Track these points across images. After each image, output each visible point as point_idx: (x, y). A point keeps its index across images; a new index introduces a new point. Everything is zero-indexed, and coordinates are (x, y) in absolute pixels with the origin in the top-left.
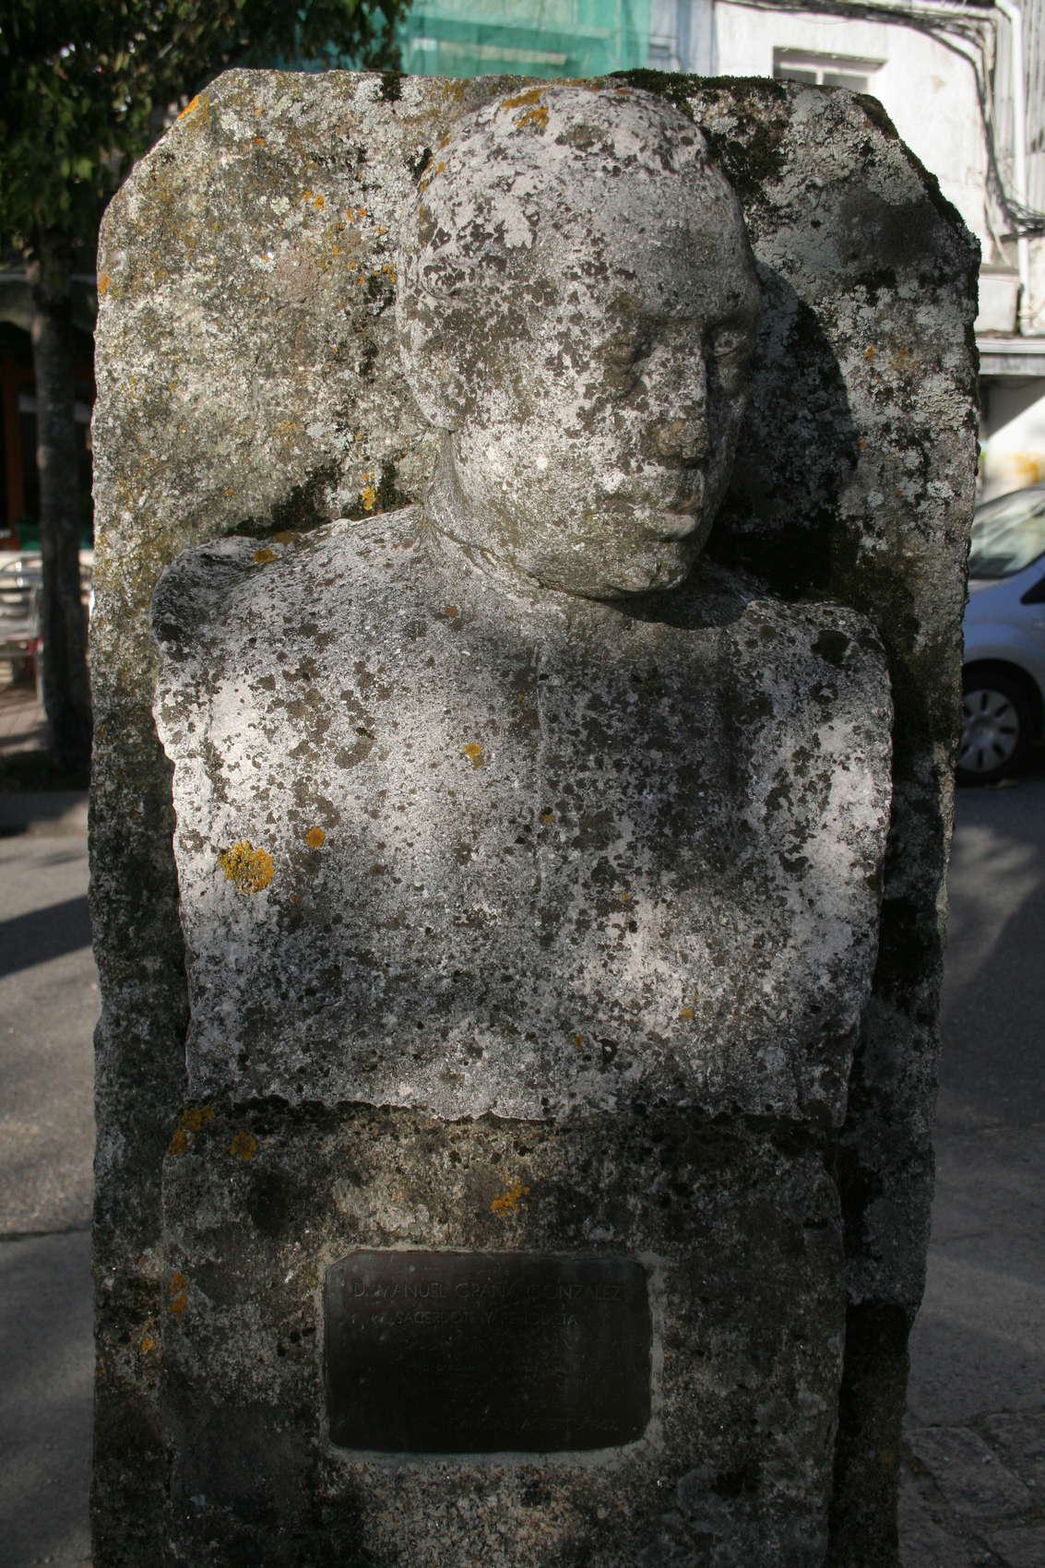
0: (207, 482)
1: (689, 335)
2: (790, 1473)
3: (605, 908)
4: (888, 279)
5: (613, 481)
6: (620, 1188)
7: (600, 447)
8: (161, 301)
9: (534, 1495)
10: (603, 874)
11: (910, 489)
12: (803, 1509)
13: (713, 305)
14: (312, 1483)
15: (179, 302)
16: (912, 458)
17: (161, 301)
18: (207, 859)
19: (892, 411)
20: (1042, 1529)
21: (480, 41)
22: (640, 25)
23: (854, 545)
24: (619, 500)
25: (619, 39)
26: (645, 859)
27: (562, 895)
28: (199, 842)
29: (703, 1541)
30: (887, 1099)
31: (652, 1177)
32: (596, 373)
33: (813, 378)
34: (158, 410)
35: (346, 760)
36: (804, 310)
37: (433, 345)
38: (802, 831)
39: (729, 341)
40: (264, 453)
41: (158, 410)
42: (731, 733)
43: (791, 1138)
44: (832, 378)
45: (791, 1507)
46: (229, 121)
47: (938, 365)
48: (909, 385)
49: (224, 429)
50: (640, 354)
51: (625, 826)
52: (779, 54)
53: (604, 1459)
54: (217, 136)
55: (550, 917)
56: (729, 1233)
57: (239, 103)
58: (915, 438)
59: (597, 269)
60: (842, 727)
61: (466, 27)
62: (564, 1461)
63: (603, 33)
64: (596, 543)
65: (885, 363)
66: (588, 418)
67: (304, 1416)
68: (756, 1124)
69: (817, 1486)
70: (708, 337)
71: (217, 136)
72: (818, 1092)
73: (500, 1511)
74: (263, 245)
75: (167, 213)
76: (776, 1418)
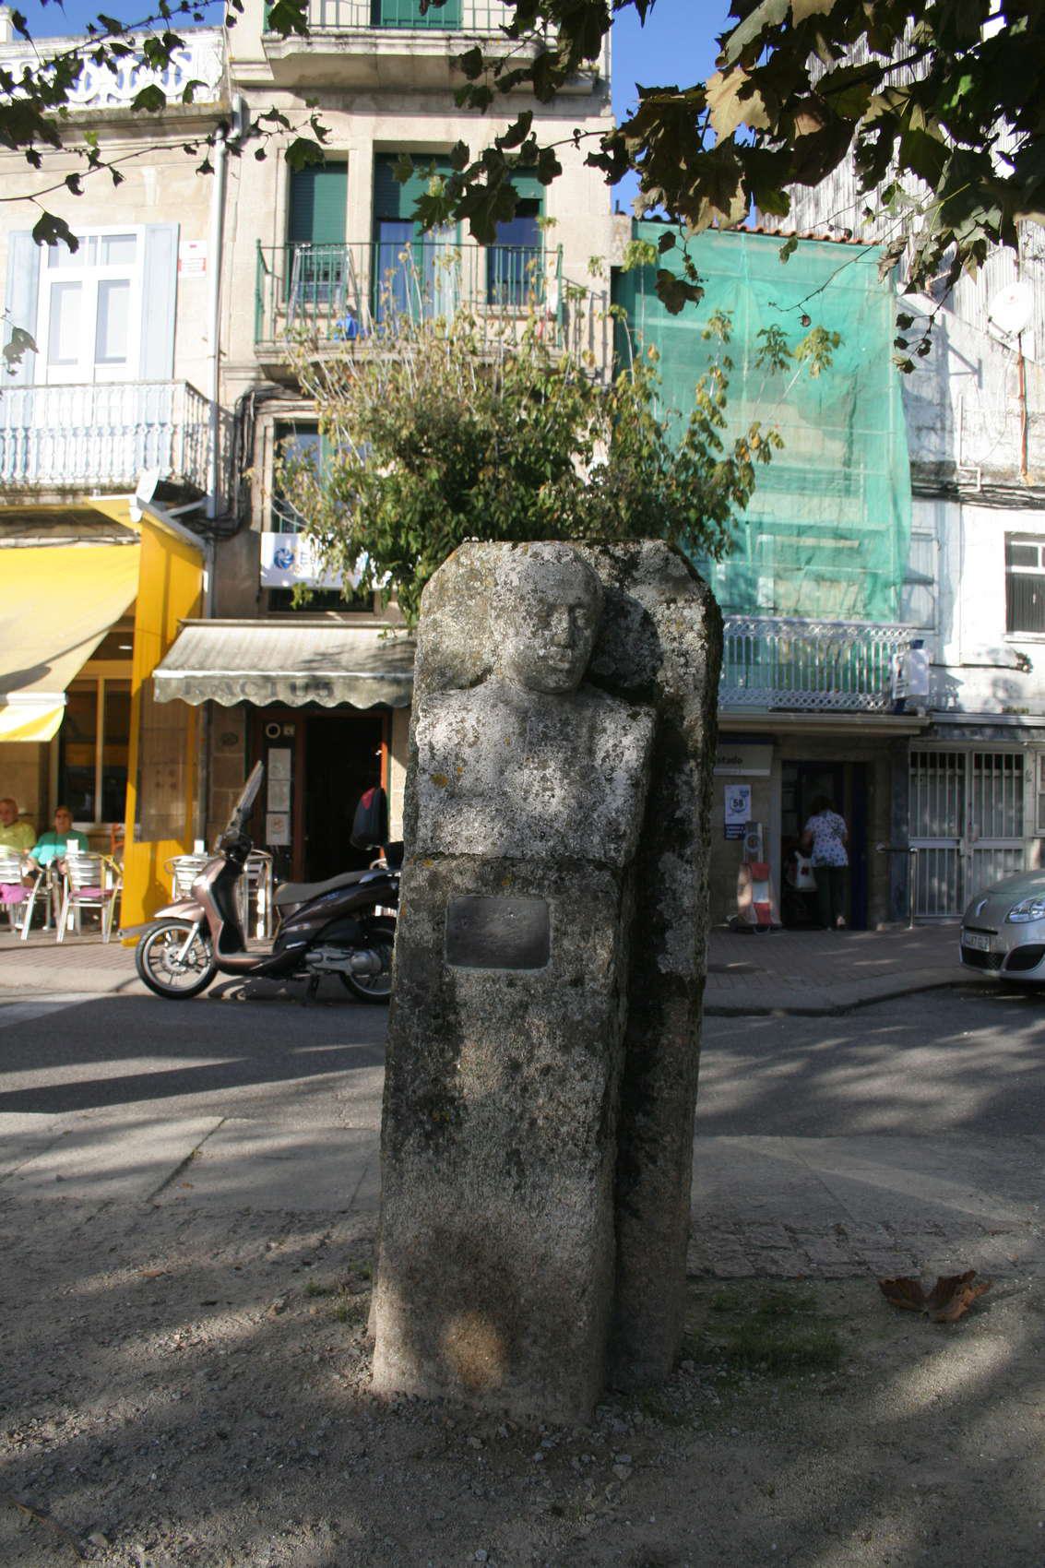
0: (449, 674)
1: (563, 609)
2: (594, 979)
3: (545, 790)
4: (674, 601)
5: (542, 652)
6: (542, 878)
7: (537, 642)
8: (438, 616)
9: (511, 984)
10: (544, 778)
11: (682, 671)
12: (599, 994)
13: (571, 600)
14: (441, 976)
15: (444, 616)
16: (682, 660)
17: (438, 616)
18: (426, 777)
19: (675, 644)
20: (1041, 1410)
21: (799, 535)
22: (906, 522)
23: (662, 690)
24: (544, 658)
25: (892, 530)
26: (558, 775)
27: (531, 785)
28: (424, 771)
29: (565, 1003)
30: (674, 892)
31: (553, 876)
32: (536, 620)
33: (648, 634)
34: (435, 651)
35: (470, 746)
36: (646, 613)
37: (498, 617)
38: (613, 769)
39: (579, 612)
40: (468, 664)
41: (435, 651)
42: (591, 738)
43: (600, 866)
44: (654, 634)
45: (595, 993)
46: (463, 559)
47: (692, 629)
48: (682, 636)
49: (456, 656)
50: (549, 615)
51: (552, 764)
52: (1009, 536)
53: (535, 972)
54: (458, 563)
55: (526, 792)
56: (575, 893)
57: (466, 553)
58: (684, 654)
59: (535, 591)
60: (630, 737)
61: (790, 527)
62: (521, 972)
63: (882, 527)
64: (539, 672)
65: (673, 629)
66: (534, 634)
67: (439, 953)
68: (589, 861)
69: (603, 985)
70: (571, 610)
71: (458, 563)
72: (613, 854)
73: (499, 990)
74: (471, 597)
75: (442, 588)
76: (590, 959)
